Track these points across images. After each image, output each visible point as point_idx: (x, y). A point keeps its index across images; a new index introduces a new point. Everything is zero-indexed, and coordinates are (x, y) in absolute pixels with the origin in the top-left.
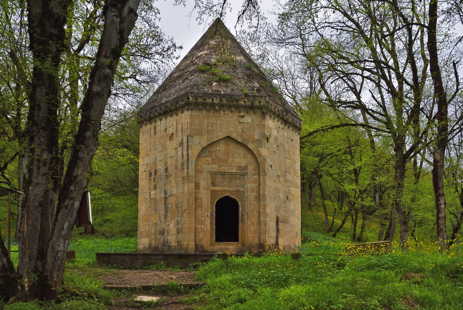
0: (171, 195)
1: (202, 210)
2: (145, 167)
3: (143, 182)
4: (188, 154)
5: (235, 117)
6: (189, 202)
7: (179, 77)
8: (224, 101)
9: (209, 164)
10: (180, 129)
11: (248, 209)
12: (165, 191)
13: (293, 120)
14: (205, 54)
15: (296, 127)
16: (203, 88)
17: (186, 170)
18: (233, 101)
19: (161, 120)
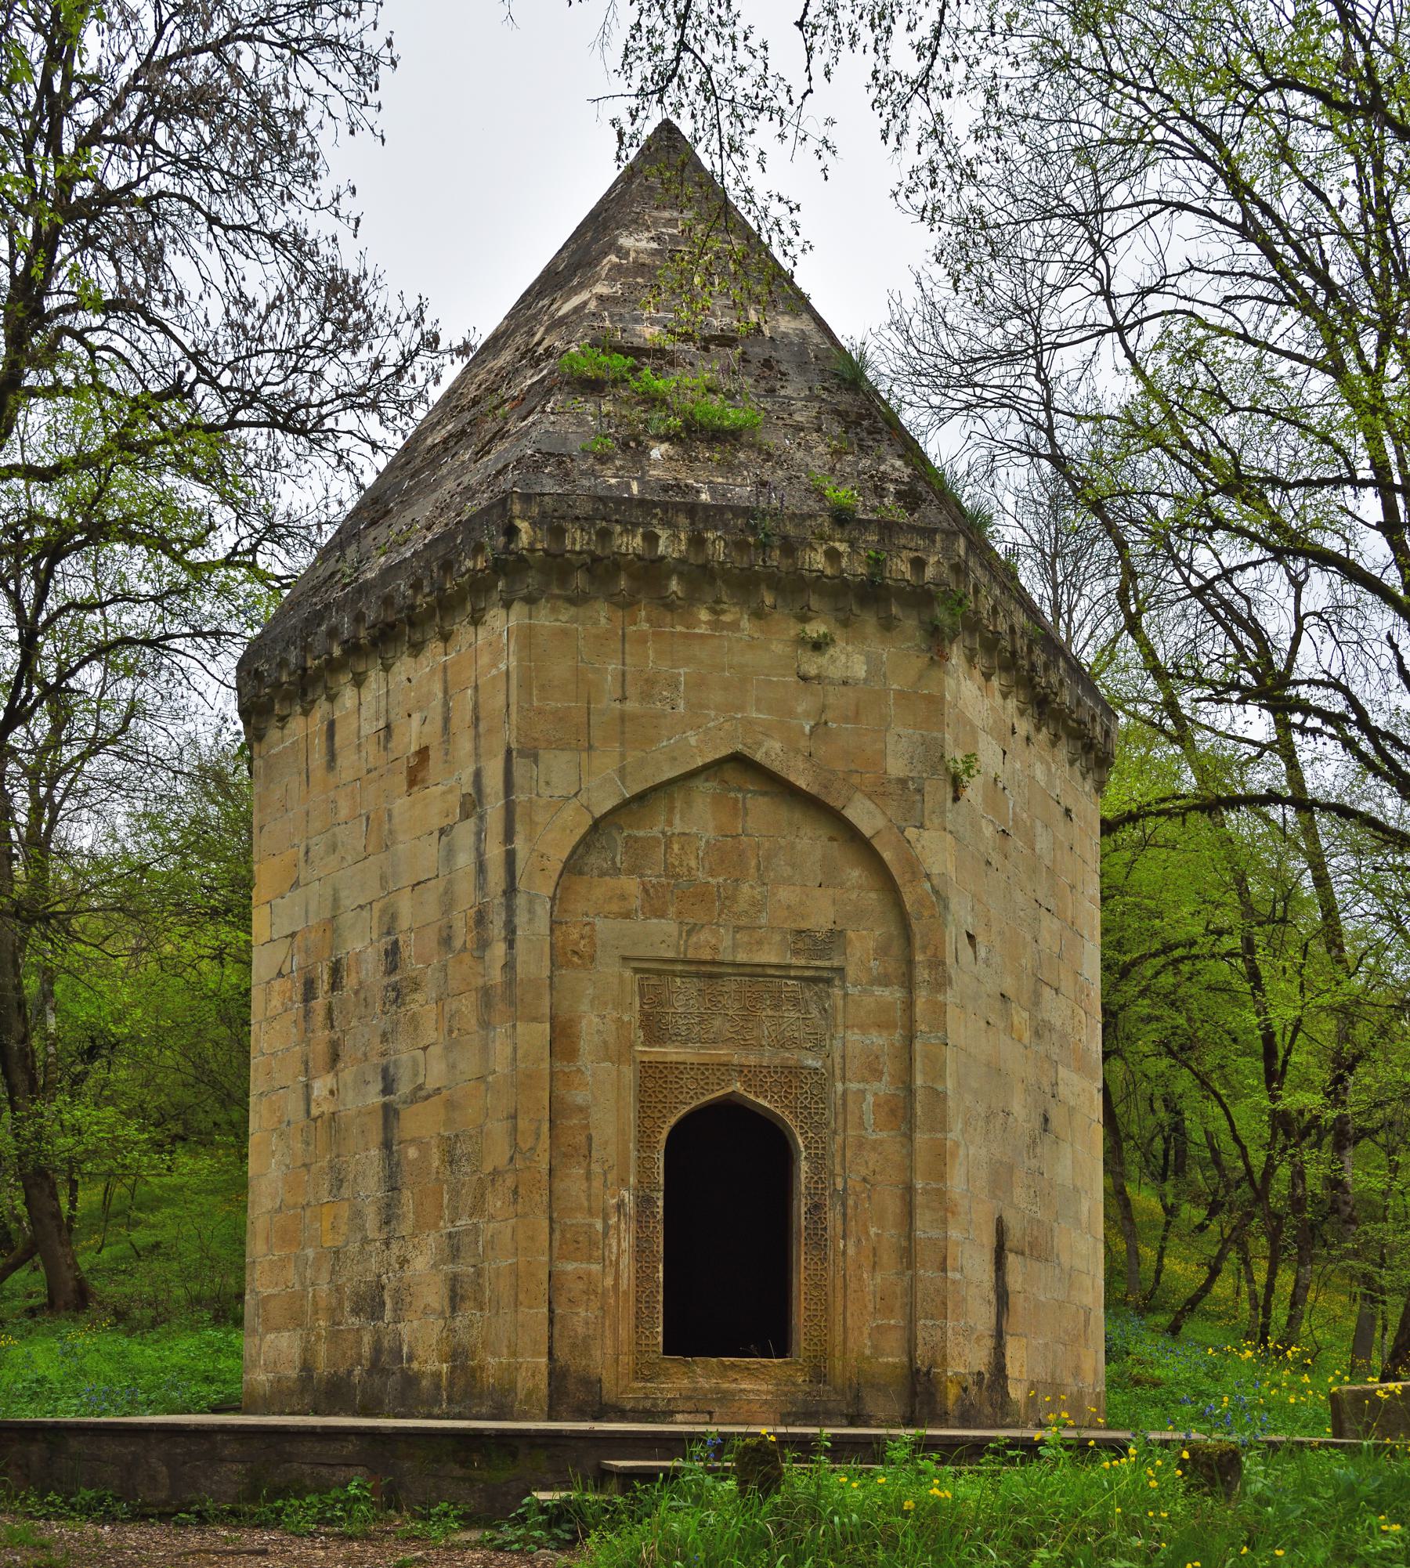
0: (418, 1095)
1: (588, 1176)
2: (281, 950)
3: (273, 1035)
4: (510, 857)
5: (777, 648)
6: (515, 1128)
7: (460, 436)
8: (718, 548)
9: (627, 915)
10: (462, 715)
11: (843, 1176)
12: (385, 1071)
13: (1079, 703)
14: (600, 298)
15: (1089, 747)
16: (593, 473)
17: (499, 949)
18: (764, 546)
19: (359, 681)
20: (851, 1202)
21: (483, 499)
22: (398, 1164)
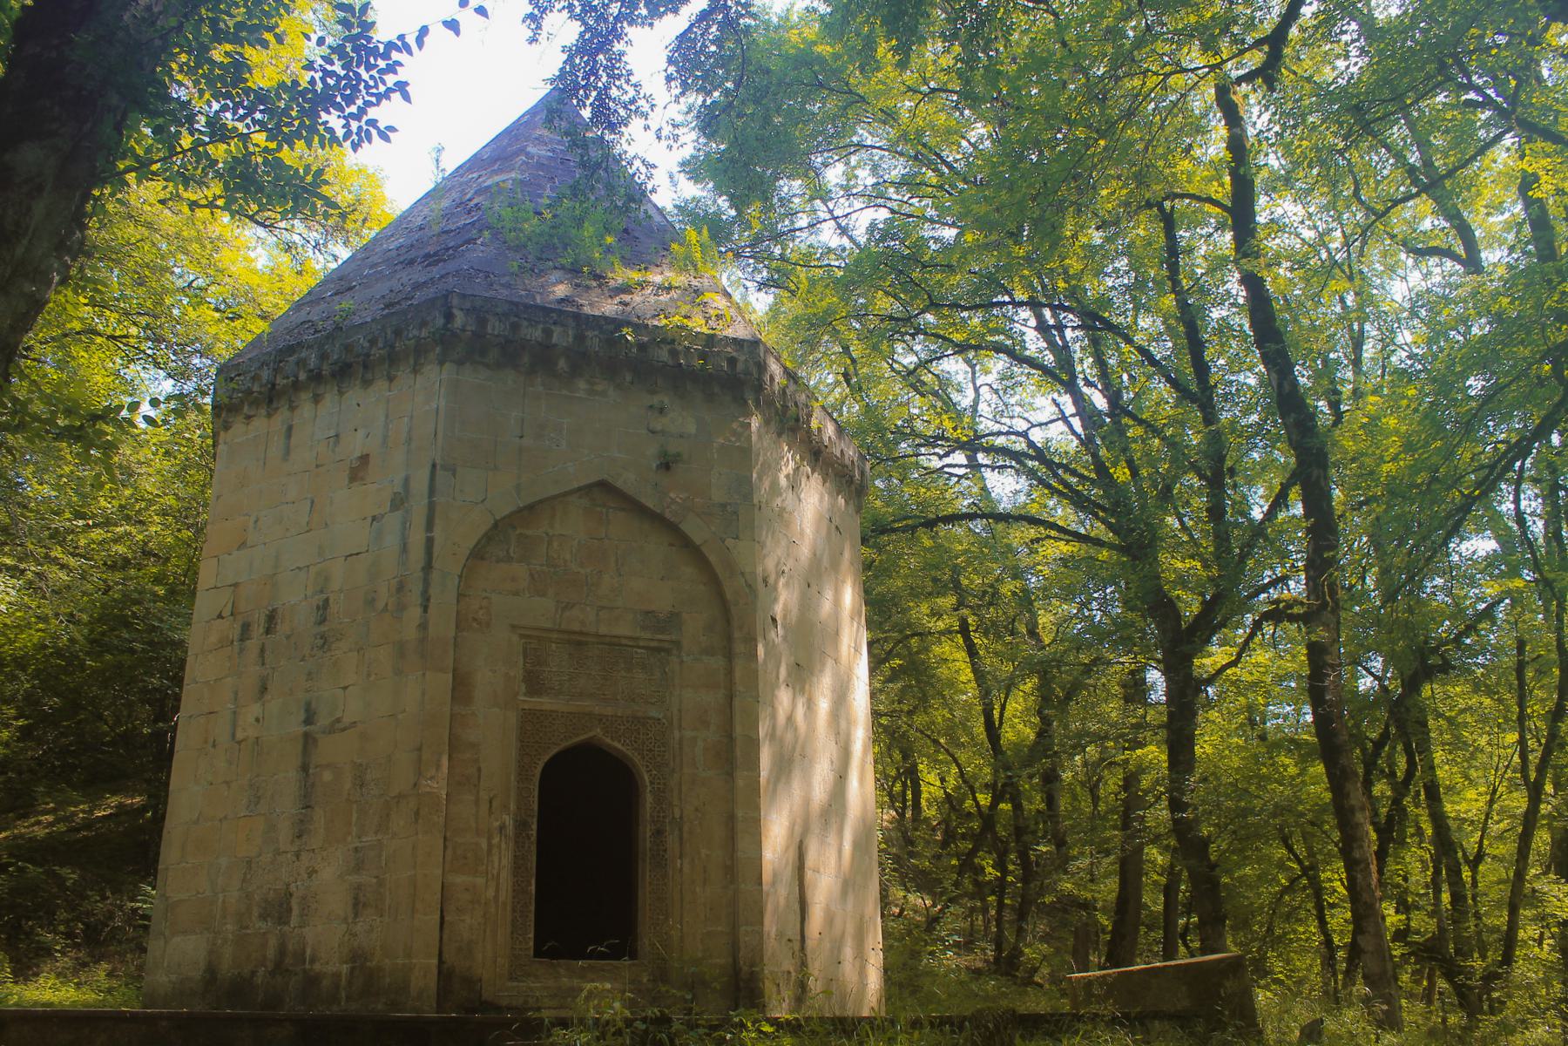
0: (335, 727)
1: (477, 802)
4: (430, 542)
9: (516, 594)
17: (415, 613)
19: (317, 399)
20: (686, 828)
21: (430, 292)
22: (313, 785)
